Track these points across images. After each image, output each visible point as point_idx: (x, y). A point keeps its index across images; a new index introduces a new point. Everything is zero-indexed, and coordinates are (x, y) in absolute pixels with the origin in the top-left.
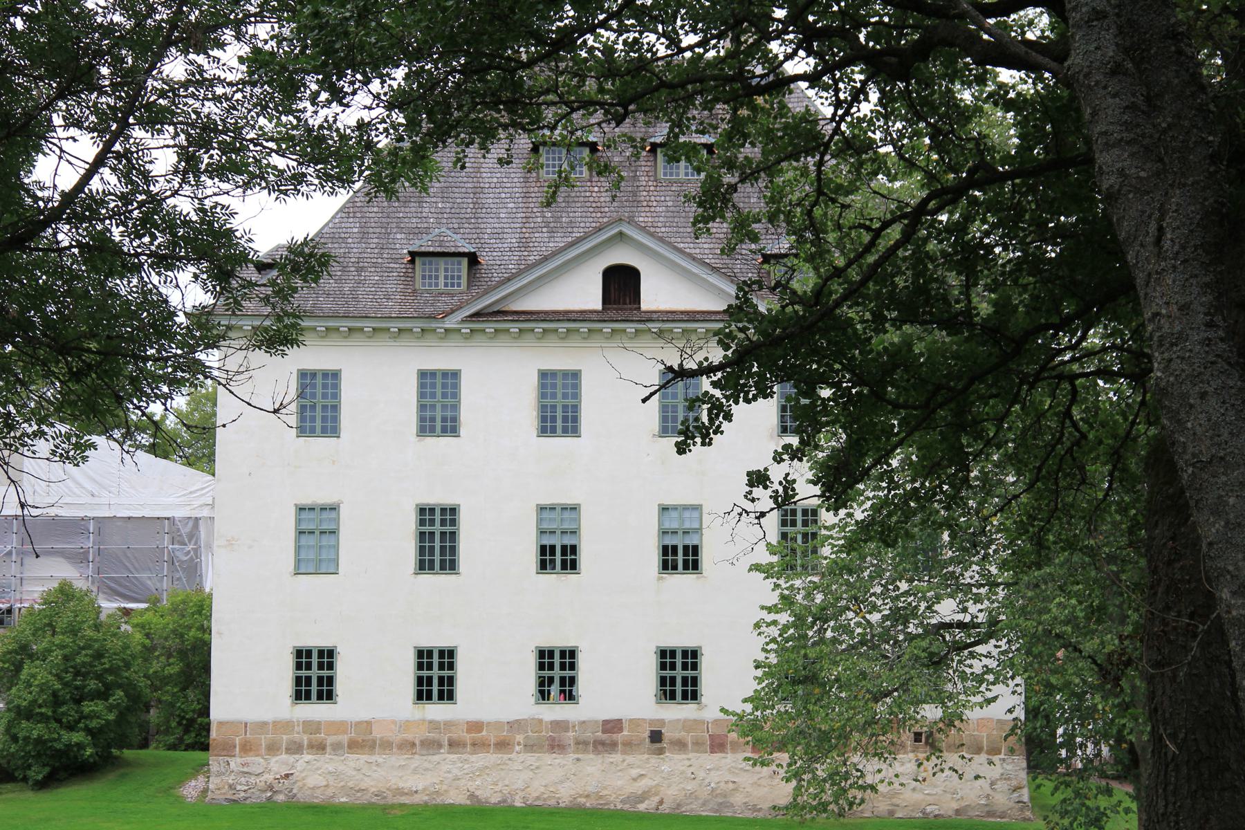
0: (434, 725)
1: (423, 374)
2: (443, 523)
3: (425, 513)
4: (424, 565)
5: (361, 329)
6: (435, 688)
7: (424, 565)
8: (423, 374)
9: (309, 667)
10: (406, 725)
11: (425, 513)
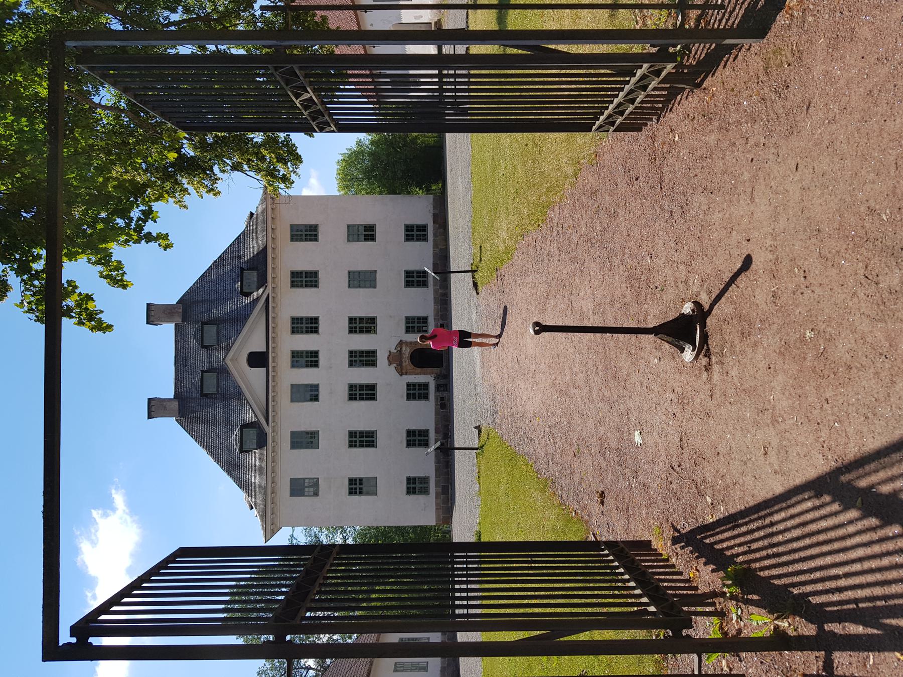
0: (435, 235)
1: (292, 495)
2: (356, 437)
3: (352, 444)
4: (373, 397)
5: (273, 457)
6: (421, 233)
7: (373, 397)
8: (292, 495)
9: (414, 441)
10: (435, 291)
11: (352, 444)
